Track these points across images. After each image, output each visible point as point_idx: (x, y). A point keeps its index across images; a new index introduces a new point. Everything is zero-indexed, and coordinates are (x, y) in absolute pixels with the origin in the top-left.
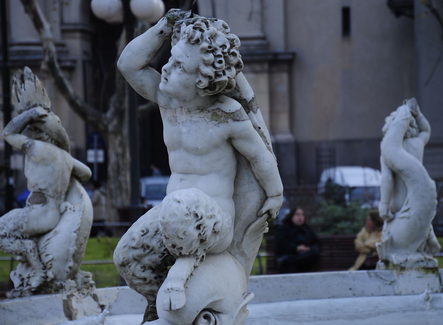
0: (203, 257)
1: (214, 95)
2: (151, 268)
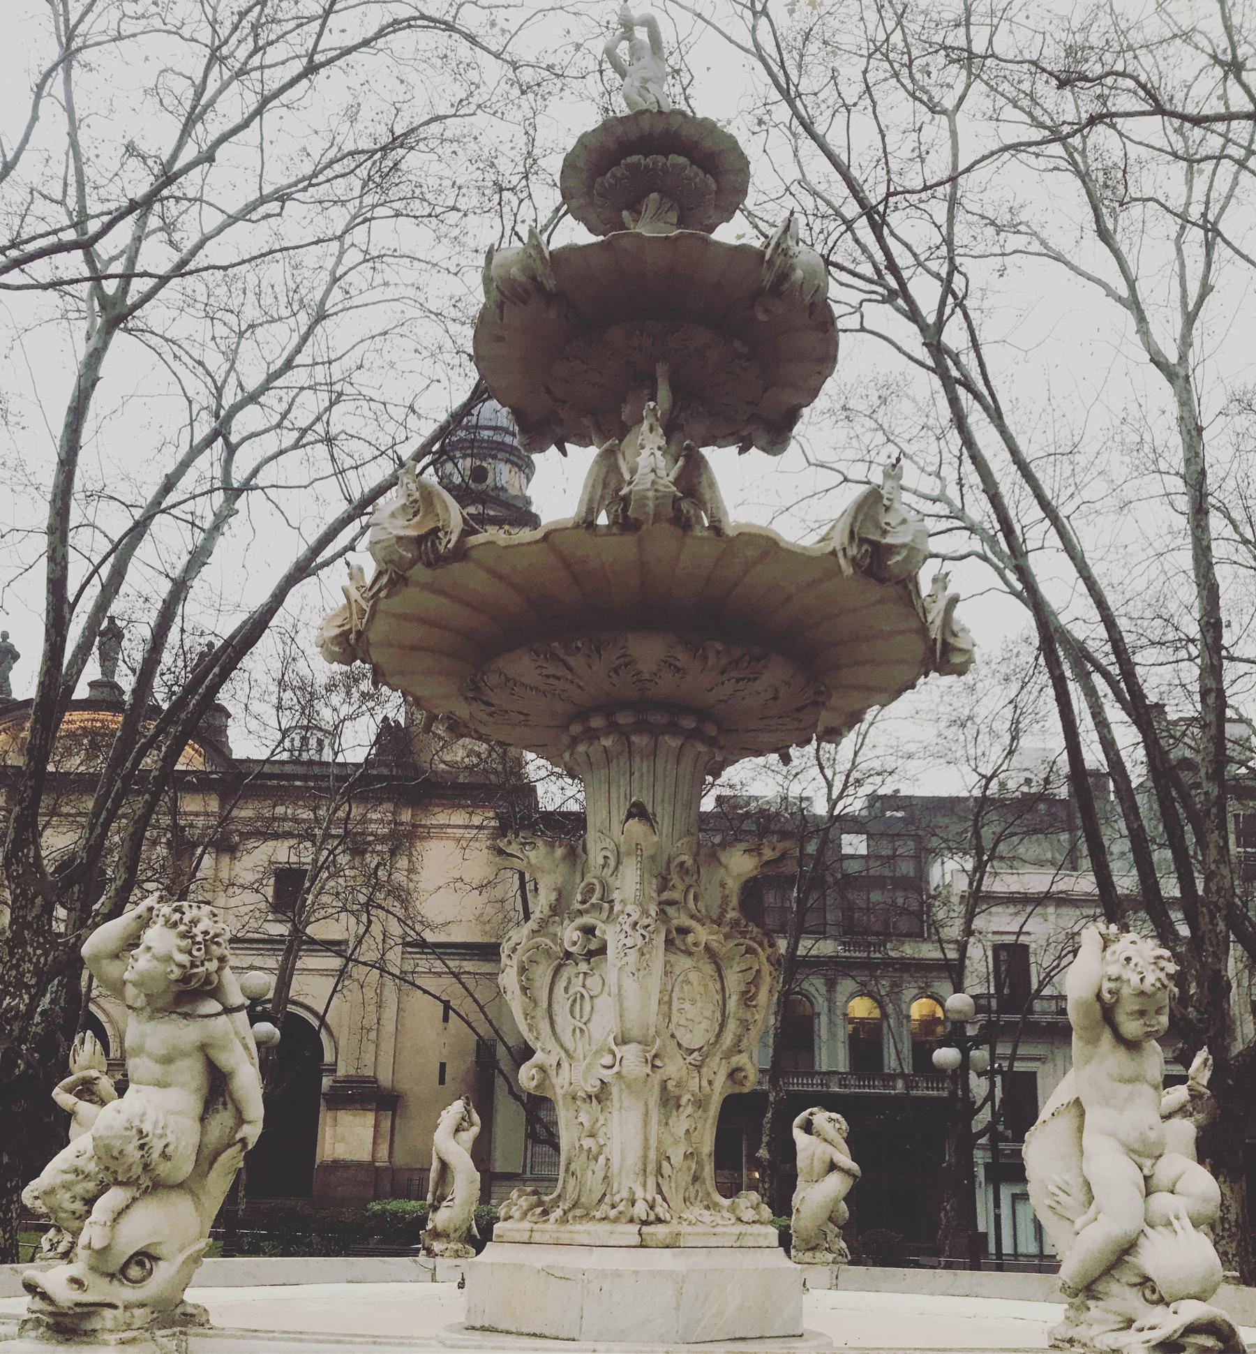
0: (148, 1187)
1: (187, 993)
2: (83, 1199)
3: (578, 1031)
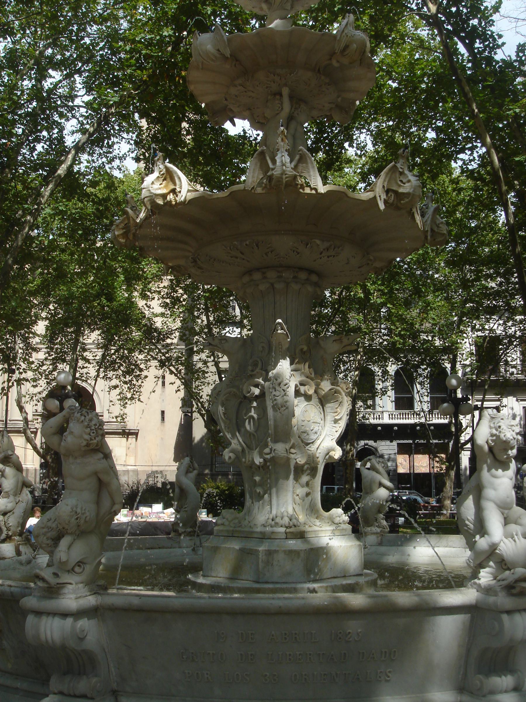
3: (252, 436)
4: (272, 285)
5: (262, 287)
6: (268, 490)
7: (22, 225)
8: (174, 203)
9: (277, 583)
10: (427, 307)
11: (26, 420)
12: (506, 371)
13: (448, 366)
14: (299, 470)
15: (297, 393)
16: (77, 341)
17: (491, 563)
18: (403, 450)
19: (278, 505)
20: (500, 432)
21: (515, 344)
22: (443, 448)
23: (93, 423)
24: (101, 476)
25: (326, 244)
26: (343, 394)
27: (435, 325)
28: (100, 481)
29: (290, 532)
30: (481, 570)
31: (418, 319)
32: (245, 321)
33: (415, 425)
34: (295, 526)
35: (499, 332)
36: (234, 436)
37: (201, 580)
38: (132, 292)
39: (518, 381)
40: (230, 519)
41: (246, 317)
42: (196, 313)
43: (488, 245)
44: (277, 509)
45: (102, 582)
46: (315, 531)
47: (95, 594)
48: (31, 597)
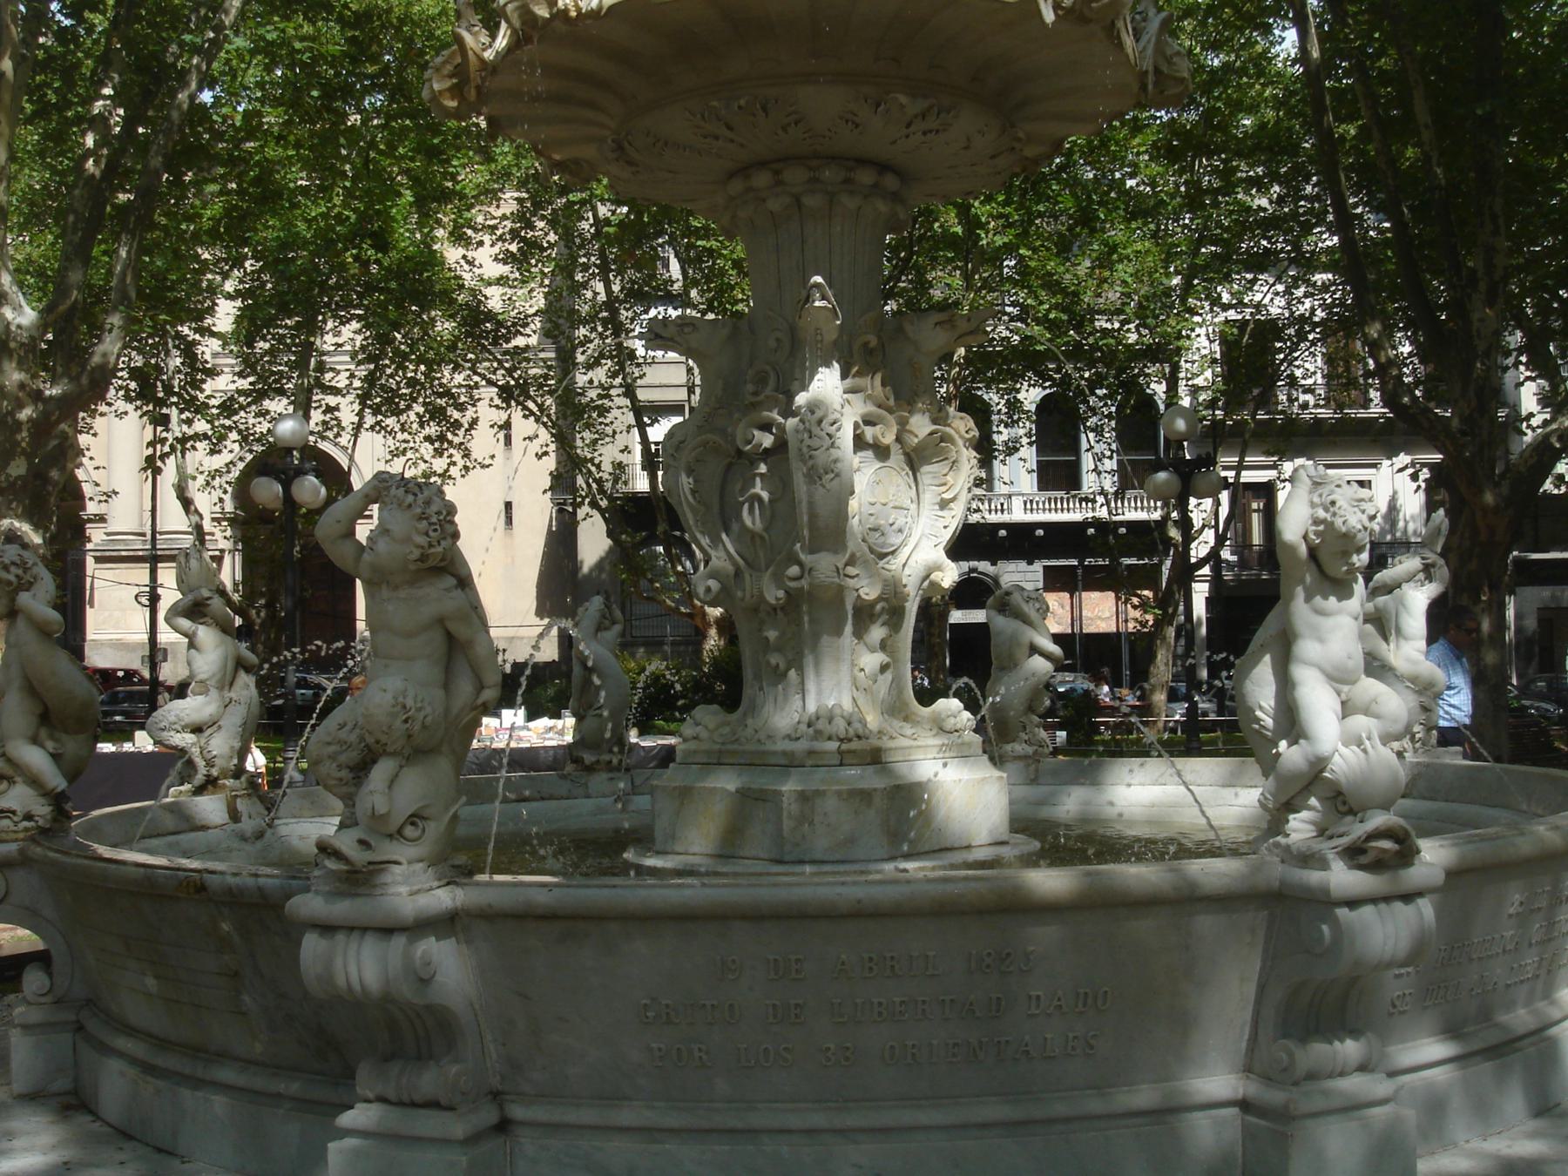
3: (758, 541)
4: (797, 200)
5: (774, 205)
6: (797, 663)
7: (182, 77)
8: (574, 14)
9: (823, 862)
10: (1110, 254)
11: (199, 532)
12: (1291, 400)
13: (1159, 389)
14: (864, 615)
15: (860, 443)
16: (308, 347)
17: (1313, 801)
18: (1057, 580)
19: (819, 693)
20: (1334, 514)
21: (1311, 337)
22: (1149, 577)
23: (434, 508)
24: (453, 627)
25: (921, 105)
26: (960, 442)
27: (1128, 295)
28: (450, 637)
29: (849, 752)
30: (1291, 817)
31: (1090, 282)
32: (694, 293)
33: (1084, 525)
34: (859, 737)
35: (1274, 311)
36: (716, 541)
37: (651, 862)
38: (432, 229)
39: (1318, 421)
40: (711, 726)
41: (695, 283)
42: (579, 277)
43: (1252, 109)
44: (818, 700)
45: (461, 859)
46: (903, 748)
47: (448, 884)
48: (310, 895)
